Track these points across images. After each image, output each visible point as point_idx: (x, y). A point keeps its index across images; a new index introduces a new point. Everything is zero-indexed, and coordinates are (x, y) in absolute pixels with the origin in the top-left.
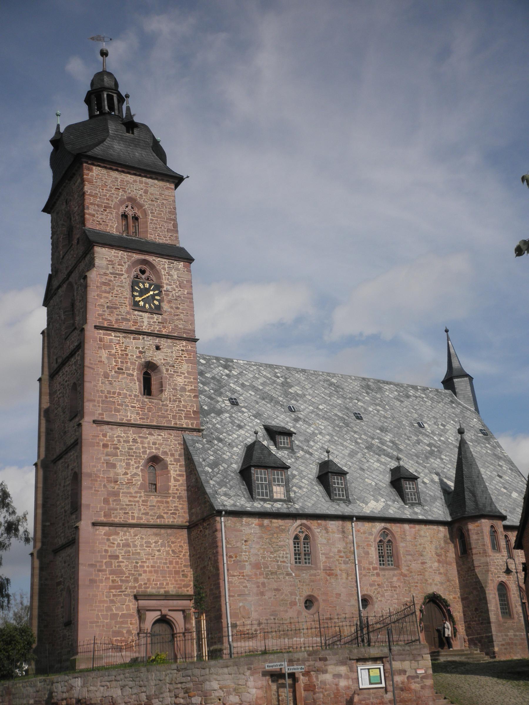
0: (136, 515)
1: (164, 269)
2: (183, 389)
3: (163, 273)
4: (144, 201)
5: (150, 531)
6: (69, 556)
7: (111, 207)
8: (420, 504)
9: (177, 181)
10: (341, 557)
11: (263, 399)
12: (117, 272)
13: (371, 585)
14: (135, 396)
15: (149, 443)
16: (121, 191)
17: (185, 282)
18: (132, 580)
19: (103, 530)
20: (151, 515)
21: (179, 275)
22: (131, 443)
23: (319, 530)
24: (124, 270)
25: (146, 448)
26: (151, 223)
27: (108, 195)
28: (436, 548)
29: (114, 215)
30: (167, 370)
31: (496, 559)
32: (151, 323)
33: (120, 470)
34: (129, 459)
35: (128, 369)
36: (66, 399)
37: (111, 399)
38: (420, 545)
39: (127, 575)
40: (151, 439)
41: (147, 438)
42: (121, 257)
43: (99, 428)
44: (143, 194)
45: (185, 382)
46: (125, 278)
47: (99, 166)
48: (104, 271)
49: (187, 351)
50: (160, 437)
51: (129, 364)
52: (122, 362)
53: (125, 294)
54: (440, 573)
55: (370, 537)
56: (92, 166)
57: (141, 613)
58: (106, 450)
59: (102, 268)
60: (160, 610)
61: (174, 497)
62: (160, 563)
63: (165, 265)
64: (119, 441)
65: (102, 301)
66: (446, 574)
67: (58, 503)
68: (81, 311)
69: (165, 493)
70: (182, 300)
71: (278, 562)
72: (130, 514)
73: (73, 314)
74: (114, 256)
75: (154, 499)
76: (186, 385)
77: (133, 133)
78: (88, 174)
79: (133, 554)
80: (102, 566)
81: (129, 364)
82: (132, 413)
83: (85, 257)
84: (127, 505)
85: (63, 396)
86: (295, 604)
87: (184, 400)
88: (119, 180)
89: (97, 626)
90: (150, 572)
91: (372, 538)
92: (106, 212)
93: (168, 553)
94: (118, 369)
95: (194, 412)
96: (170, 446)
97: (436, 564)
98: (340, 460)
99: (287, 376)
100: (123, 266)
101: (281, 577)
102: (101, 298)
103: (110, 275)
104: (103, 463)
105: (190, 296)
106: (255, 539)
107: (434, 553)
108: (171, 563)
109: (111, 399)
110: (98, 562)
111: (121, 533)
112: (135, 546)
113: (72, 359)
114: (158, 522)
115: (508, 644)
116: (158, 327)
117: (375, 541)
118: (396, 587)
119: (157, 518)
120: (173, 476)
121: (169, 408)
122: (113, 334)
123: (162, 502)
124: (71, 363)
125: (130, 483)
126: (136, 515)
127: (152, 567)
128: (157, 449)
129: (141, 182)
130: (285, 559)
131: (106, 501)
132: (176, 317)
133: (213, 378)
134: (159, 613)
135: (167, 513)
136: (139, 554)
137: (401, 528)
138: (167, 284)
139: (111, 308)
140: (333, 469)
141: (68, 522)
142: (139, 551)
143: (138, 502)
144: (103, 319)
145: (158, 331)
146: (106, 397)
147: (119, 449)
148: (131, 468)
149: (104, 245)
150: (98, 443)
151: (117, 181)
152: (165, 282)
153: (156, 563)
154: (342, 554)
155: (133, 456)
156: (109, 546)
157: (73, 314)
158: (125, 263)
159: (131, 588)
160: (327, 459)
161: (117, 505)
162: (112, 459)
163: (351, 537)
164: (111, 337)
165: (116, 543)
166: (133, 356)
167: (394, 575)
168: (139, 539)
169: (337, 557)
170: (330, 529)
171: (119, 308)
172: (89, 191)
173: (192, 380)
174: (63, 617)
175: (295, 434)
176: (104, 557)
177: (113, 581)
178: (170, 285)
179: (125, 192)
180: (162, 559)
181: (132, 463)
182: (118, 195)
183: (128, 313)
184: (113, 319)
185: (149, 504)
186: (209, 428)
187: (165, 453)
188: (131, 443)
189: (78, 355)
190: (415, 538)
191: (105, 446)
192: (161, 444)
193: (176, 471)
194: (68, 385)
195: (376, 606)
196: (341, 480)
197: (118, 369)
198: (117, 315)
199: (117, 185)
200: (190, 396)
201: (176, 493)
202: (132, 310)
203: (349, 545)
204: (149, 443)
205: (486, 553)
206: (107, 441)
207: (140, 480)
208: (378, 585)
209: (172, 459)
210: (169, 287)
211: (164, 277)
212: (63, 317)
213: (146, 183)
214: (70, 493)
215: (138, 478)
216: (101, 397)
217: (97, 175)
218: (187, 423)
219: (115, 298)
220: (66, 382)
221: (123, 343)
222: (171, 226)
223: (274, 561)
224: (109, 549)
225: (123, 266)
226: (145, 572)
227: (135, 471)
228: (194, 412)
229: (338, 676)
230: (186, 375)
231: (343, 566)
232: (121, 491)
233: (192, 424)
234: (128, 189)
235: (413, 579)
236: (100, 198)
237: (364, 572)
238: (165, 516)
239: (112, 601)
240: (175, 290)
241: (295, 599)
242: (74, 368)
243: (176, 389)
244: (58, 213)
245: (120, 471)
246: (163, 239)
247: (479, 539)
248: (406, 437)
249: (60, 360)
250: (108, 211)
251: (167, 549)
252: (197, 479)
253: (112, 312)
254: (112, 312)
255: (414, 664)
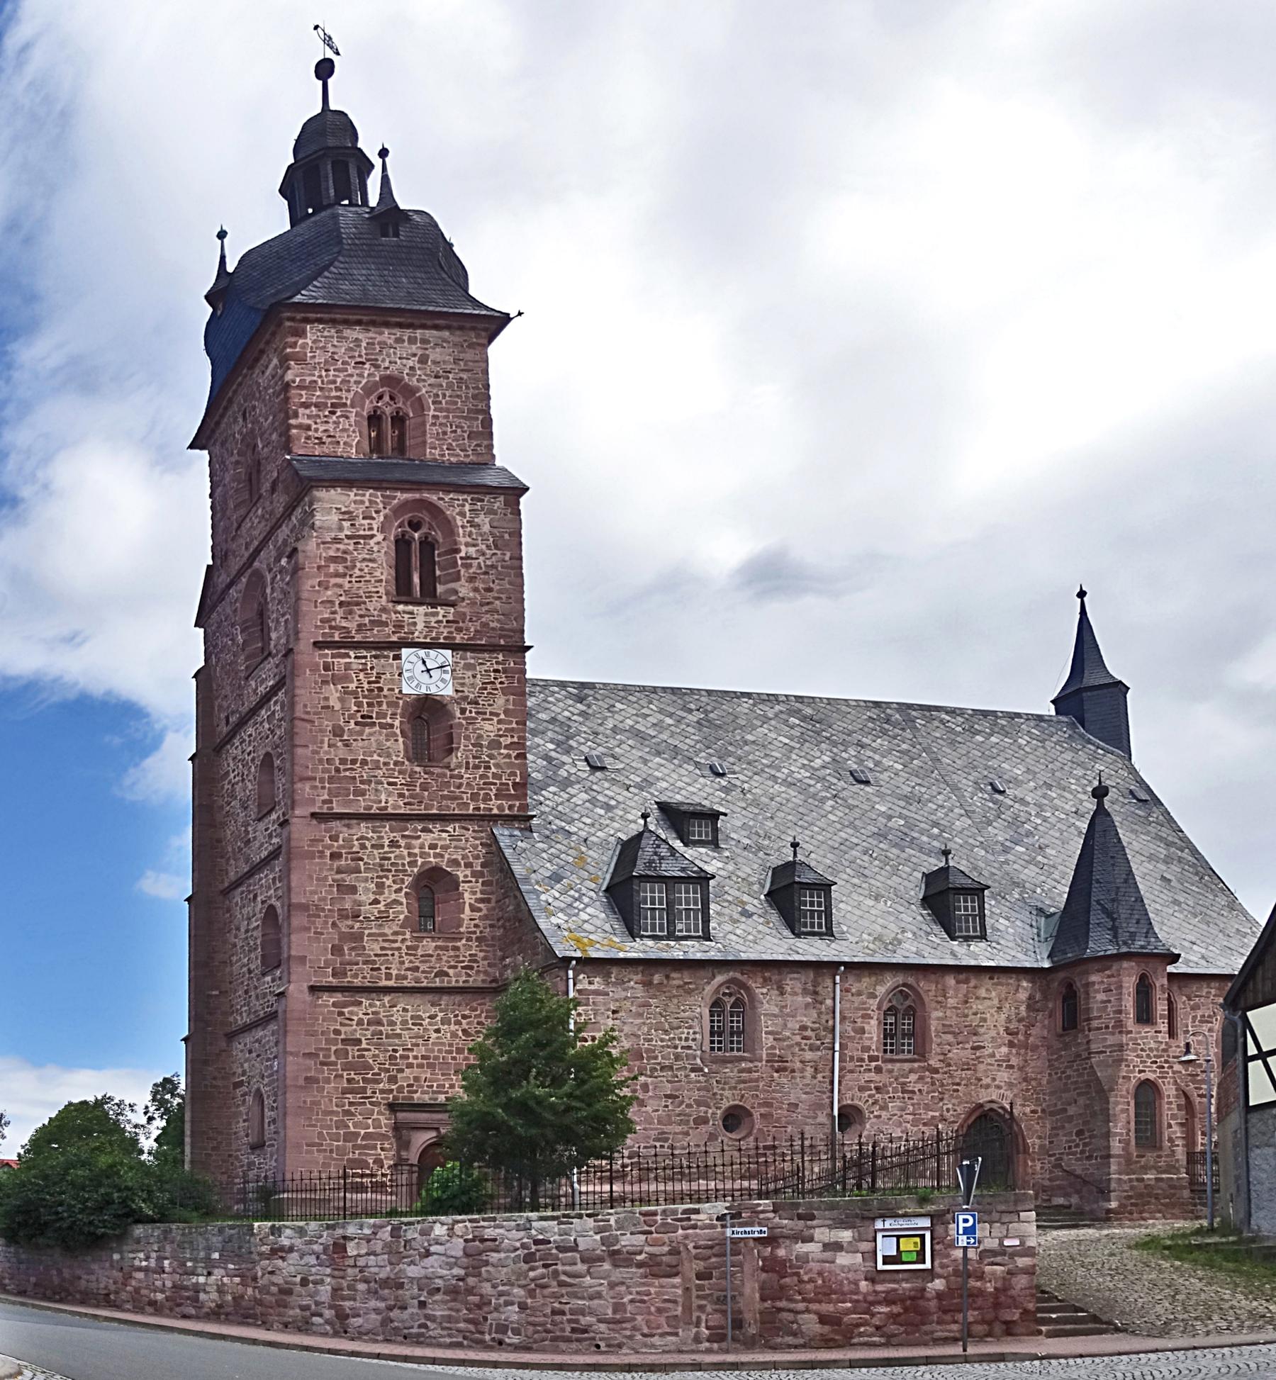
0: (396, 970)
1: (462, 514)
2: (495, 744)
3: (460, 523)
4: (418, 380)
5: (417, 999)
6: (259, 1041)
7: (345, 405)
8: (983, 937)
9: (493, 327)
10: (804, 1038)
11: (658, 754)
12: (362, 533)
13: (861, 1089)
14: (396, 763)
15: (422, 847)
16: (367, 366)
17: (507, 536)
18: (385, 1080)
19: (329, 999)
20: (423, 972)
21: (495, 524)
22: (386, 849)
23: (765, 991)
24: (375, 527)
25: (416, 855)
26: (434, 424)
27: (339, 380)
28: (1009, 1020)
29: (352, 420)
30: (463, 711)
31: (1142, 1038)
32: (433, 624)
33: (365, 896)
34: (381, 877)
35: (381, 715)
36: (249, 784)
37: (347, 773)
38: (975, 1014)
39: (376, 1071)
40: (427, 838)
41: (419, 837)
42: (370, 501)
43: (323, 826)
44: (417, 366)
45: (499, 730)
46: (378, 543)
47: (320, 321)
48: (333, 535)
49: (505, 671)
50: (445, 835)
51: (384, 707)
52: (369, 705)
53: (378, 574)
54: (1012, 1067)
55: (871, 1001)
56: (302, 325)
57: (401, 1132)
58: (336, 864)
59: (329, 529)
60: (437, 1129)
61: (469, 939)
62: (440, 1051)
63: (463, 506)
64: (363, 847)
65: (329, 593)
66: (1021, 1069)
67: (234, 959)
68: (282, 620)
69: (450, 934)
70: (500, 573)
71: (676, 1047)
72: (384, 971)
73: (262, 630)
74: (355, 502)
75: (428, 946)
76: (501, 736)
77: (397, 235)
78: (295, 343)
79: (388, 1036)
80: (329, 1056)
81: (384, 707)
82: (389, 794)
83: (291, 514)
84: (376, 955)
85: (243, 780)
86: (705, 1121)
87: (497, 765)
88: (364, 344)
89: (319, 1151)
90: (420, 1066)
91: (874, 1003)
92: (334, 418)
93: (454, 1035)
94: (363, 717)
95: (515, 784)
96: (464, 849)
97: (1004, 1050)
98: (819, 860)
99: (709, 708)
100: (373, 519)
101: (681, 1074)
102: (327, 588)
103: (346, 541)
104: (331, 886)
105: (516, 563)
106: (633, 1009)
107: (1002, 1030)
108: (459, 1051)
109: (347, 773)
110: (322, 1049)
111: (366, 1002)
112: (392, 1023)
113: (263, 712)
114: (438, 983)
115: (1141, 1195)
116: (446, 631)
117: (879, 1009)
118: (913, 1092)
119: (436, 976)
120: (468, 901)
121: (464, 781)
122: (352, 654)
123: (446, 949)
124: (259, 719)
125: (383, 918)
126: (394, 972)
127: (423, 1057)
128: (436, 855)
129: (412, 341)
130: (691, 1043)
131: (337, 950)
132: (486, 608)
133: (553, 720)
134: (434, 1134)
135: (455, 967)
136: (399, 1036)
137: (937, 983)
138: (467, 545)
139: (349, 604)
140: (807, 878)
141: (256, 988)
142: (399, 1031)
143: (399, 949)
144: (331, 628)
145: (445, 638)
146: (337, 770)
147: (362, 859)
148: (386, 891)
149: (333, 483)
150: (322, 852)
151: (360, 346)
152: (462, 540)
153: (433, 1051)
154: (809, 1033)
155: (390, 871)
156: (342, 1024)
157: (262, 630)
158: (377, 512)
159: (382, 1092)
160: (791, 859)
161: (359, 955)
162: (348, 879)
163: (829, 1002)
164: (348, 660)
165: (355, 1018)
166: (393, 690)
167: (911, 1071)
168: (400, 1011)
169: (798, 1038)
170: (788, 989)
171: (365, 603)
172: (298, 379)
173: (514, 725)
174: (247, 1136)
175: (725, 815)
176: (335, 1042)
177: (349, 1081)
178: (474, 545)
179: (377, 367)
180: (443, 1044)
181: (388, 882)
182: (361, 375)
183: (384, 610)
184: (352, 626)
185: (420, 952)
186: (543, 813)
187: (455, 863)
188: (386, 849)
189: (276, 703)
190: (966, 1002)
191: (335, 856)
192: (445, 848)
193: (474, 893)
194: (253, 760)
195: (868, 1126)
196: (819, 897)
197: (363, 717)
198: (361, 616)
199: (360, 356)
200: (509, 756)
201: (475, 933)
202: (390, 605)
203: (824, 1017)
204: (422, 847)
205: (1121, 1026)
206: (339, 847)
207: (402, 912)
208: (877, 1088)
209: (468, 872)
210: (472, 550)
211: (461, 530)
212: (240, 639)
213: (424, 341)
214: (259, 942)
215: (399, 908)
216: (328, 771)
217: (314, 342)
218: (500, 807)
219: (358, 585)
220: (249, 754)
221: (372, 668)
222: (477, 426)
223: (668, 1047)
224: (343, 1029)
225: (373, 519)
226: (410, 1066)
227: (394, 896)
228: (515, 784)
229: (837, 1247)
230: (502, 716)
231: (809, 1055)
232: (366, 932)
233: (510, 807)
234: (383, 360)
235: (951, 1076)
236: (321, 389)
237: (850, 1065)
238: (451, 972)
239: (347, 1113)
240: (484, 554)
241: (706, 1112)
242: (267, 726)
243: (481, 746)
244: (223, 444)
245: (363, 898)
246: (458, 455)
247: (1109, 1001)
248: (963, 812)
249: (233, 719)
250: (339, 414)
251: (453, 1027)
252: (518, 905)
253: (351, 612)
254: (351, 612)
255: (998, 1229)
